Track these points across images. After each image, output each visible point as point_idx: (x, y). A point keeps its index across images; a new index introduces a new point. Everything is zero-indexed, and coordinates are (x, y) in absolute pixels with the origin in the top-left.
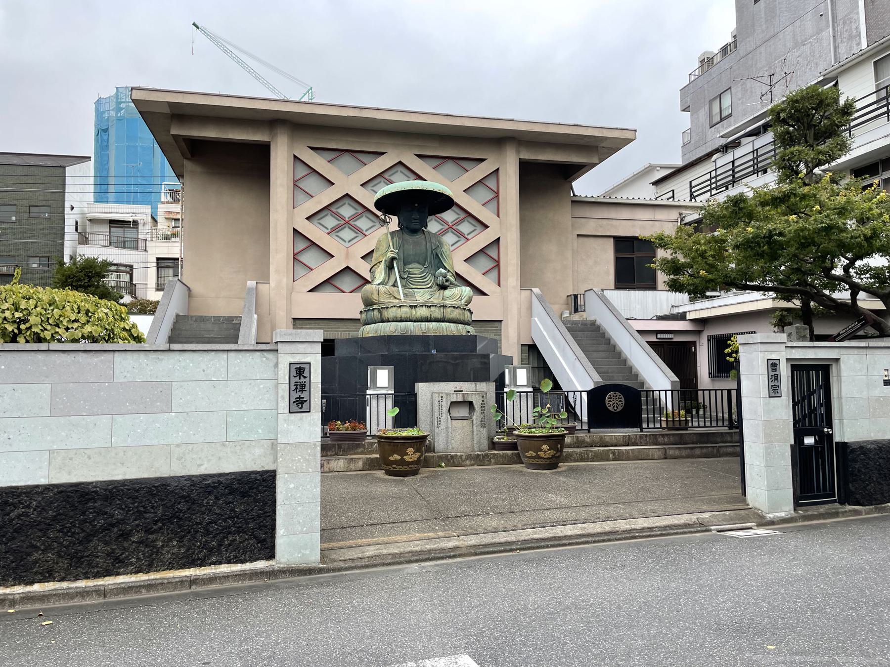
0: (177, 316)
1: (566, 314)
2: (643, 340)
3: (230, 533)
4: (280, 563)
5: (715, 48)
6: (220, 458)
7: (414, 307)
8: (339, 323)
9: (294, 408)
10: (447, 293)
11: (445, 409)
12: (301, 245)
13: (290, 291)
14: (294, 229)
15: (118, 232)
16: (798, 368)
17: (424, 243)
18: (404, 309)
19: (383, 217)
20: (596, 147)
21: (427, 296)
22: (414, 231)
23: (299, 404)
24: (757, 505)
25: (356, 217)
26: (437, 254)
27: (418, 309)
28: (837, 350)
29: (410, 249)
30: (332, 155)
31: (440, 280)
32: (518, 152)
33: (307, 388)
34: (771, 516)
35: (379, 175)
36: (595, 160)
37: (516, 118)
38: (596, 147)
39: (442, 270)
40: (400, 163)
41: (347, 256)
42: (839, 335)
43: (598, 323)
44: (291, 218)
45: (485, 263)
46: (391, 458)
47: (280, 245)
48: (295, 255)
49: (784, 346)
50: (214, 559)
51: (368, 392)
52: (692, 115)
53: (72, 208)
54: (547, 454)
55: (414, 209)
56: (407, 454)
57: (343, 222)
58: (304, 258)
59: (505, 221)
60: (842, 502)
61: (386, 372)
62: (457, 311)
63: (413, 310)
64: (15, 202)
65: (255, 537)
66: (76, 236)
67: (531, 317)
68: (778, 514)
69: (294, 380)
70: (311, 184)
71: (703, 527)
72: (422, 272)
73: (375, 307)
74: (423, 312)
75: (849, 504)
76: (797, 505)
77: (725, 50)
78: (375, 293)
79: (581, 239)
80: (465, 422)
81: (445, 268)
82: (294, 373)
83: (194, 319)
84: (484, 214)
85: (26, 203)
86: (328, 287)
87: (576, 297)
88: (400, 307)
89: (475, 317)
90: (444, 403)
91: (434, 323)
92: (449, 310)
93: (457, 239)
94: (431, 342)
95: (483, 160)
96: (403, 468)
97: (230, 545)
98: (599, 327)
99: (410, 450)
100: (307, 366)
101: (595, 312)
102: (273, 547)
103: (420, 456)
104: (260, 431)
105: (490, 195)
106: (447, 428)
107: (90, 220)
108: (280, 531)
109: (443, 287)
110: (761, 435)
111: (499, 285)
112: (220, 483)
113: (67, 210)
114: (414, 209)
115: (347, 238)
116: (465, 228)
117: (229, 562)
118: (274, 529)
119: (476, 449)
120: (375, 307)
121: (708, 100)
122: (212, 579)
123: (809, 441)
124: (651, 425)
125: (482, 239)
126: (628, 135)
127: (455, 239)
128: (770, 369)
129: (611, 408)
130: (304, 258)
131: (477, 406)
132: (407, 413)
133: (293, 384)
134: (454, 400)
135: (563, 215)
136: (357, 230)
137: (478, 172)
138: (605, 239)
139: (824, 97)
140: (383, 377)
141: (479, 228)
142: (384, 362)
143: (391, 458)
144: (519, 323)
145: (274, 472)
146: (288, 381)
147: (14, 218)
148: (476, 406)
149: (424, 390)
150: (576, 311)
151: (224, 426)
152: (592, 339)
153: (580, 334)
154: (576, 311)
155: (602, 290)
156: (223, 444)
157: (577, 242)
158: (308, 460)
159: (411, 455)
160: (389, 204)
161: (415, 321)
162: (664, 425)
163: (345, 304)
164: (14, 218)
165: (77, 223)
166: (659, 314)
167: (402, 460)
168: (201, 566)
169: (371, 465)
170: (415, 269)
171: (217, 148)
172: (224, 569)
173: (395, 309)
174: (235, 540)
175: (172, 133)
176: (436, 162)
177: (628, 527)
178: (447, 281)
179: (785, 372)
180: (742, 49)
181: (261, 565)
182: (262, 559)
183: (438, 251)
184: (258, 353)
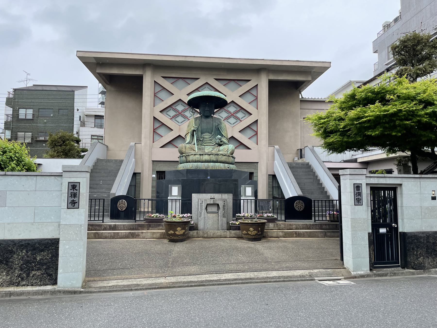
0: (98, 159)
2: (330, 173)
3: (33, 270)
4: (59, 287)
5: (391, 20)
6: (30, 231)
7: (204, 156)
8: (159, 163)
9: (70, 206)
10: (221, 148)
11: (204, 207)
12: (157, 125)
13: (151, 148)
14: (154, 117)
15: (98, 121)
16: (375, 190)
17: (212, 122)
18: (197, 156)
20: (312, 72)
21: (211, 149)
22: (207, 117)
23: (73, 203)
24: (348, 266)
25: (237, 112)
27: (204, 156)
28: (400, 179)
29: (204, 126)
30: (173, 80)
31: (218, 141)
33: (77, 196)
34: (355, 273)
36: (310, 79)
37: (265, 58)
38: (312, 72)
39: (219, 136)
40: (207, 83)
41: (180, 130)
42: (425, 171)
43: (310, 164)
44: (152, 111)
45: (250, 133)
46: (169, 232)
47: (147, 124)
48: (154, 129)
49: (365, 176)
50: (24, 283)
51: (169, 198)
52: (379, 55)
53: (78, 110)
54: (258, 232)
55: (208, 106)
56: (177, 231)
57: (178, 113)
58: (159, 131)
59: (261, 111)
60: (403, 268)
61: (177, 188)
62: (225, 157)
63: (201, 156)
64: (52, 107)
65: (47, 273)
66: (79, 122)
67: (274, 161)
68: (359, 272)
69: (70, 191)
70: (162, 95)
71: (311, 278)
72: (210, 138)
73: (184, 155)
74: (206, 157)
75: (407, 269)
76: (372, 267)
77: (396, 20)
78: (184, 148)
80: (214, 215)
81: (222, 135)
82: (70, 187)
85: (57, 108)
86: (170, 145)
87: (301, 150)
88: (195, 155)
89: (236, 160)
90: (203, 204)
92: (220, 156)
93: (236, 121)
94: (209, 173)
95: (249, 80)
96: (175, 238)
97: (33, 276)
98: (310, 166)
99: (179, 229)
100: (78, 184)
101: (309, 158)
102: (56, 279)
103: (185, 232)
104: (52, 218)
106: (205, 218)
107: (86, 115)
108: (60, 271)
109: (220, 145)
110: (350, 227)
112: (28, 244)
113: (75, 111)
114: (208, 106)
115: (180, 121)
116: (240, 115)
117: (32, 285)
118: (57, 269)
120: (184, 155)
121: (387, 46)
122: (21, 294)
123: (383, 230)
124: (321, 219)
125: (249, 121)
126: (326, 65)
127: (235, 121)
128: (355, 189)
129: (297, 209)
130: (159, 131)
131: (221, 206)
133: (69, 193)
135: (296, 108)
136: (237, 118)
139: (420, 39)
140: (175, 191)
141: (247, 115)
142: (175, 183)
143: (169, 232)
144: (267, 164)
145: (59, 239)
146: (67, 192)
147: (52, 115)
148: (220, 206)
149: (195, 197)
150: (301, 157)
151: (33, 214)
154: (301, 157)
155: (313, 147)
156: (32, 224)
158: (77, 234)
159: (179, 231)
160: (194, 103)
161: (202, 162)
162: (328, 218)
163: (172, 154)
164: (52, 115)
165: (80, 116)
166: (345, 159)
167: (175, 233)
168: (17, 286)
169: (163, 237)
170: (207, 136)
171: (122, 79)
172: (29, 288)
173: (192, 156)
174: (36, 274)
176: (226, 82)
177: (265, 276)
178: (221, 142)
179: (366, 192)
180: (404, 19)
181: (49, 288)
182: (50, 285)
183: (219, 127)
184: (53, 177)
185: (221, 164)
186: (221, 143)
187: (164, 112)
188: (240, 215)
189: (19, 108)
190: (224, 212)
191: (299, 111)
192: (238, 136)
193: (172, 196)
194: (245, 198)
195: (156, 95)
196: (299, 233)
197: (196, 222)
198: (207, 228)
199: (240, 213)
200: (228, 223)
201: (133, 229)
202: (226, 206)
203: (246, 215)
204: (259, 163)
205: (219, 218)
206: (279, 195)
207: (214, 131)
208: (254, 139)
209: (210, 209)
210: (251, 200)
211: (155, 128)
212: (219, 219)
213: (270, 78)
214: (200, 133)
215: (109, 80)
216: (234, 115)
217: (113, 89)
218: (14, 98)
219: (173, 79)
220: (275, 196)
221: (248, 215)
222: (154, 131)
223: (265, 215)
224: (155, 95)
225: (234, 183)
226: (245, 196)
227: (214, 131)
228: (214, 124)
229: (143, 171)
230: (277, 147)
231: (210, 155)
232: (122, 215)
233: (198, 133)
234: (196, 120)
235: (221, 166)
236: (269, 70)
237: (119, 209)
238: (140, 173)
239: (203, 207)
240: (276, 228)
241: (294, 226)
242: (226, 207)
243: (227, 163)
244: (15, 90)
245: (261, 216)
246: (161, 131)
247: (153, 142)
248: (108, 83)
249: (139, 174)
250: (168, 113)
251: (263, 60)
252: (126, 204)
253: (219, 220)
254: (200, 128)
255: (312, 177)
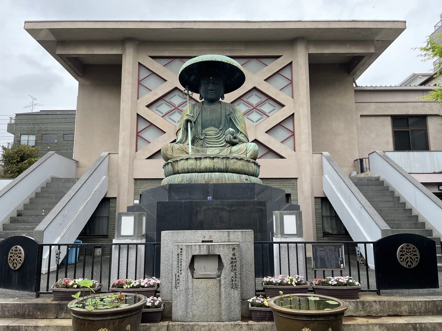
1: (354, 174)
2: (430, 192)
7: (207, 164)
10: (235, 148)
13: (133, 159)
14: (137, 114)
17: (219, 110)
18: (190, 161)
19: (186, 92)
20: (374, 39)
22: (213, 101)
26: (230, 119)
27: (202, 160)
31: (229, 137)
32: (307, 48)
35: (277, 72)
36: (372, 50)
38: (374, 39)
39: (231, 129)
43: (381, 179)
45: (282, 134)
51: (114, 241)
59: (298, 98)
62: (241, 162)
63: (198, 162)
70: (151, 82)
72: (217, 134)
73: (169, 161)
74: (206, 163)
78: (170, 149)
79: (364, 119)
80: (211, 282)
83: (64, 180)
84: (281, 97)
87: (361, 160)
88: (187, 159)
90: (184, 257)
91: (217, 173)
92: (232, 161)
94: (210, 190)
98: (383, 182)
101: (379, 169)
105: (286, 83)
106: (187, 289)
109: (234, 144)
111: (295, 151)
116: (267, 108)
119: (224, 318)
120: (169, 161)
125: (279, 115)
126: (400, 26)
127: (259, 117)
129: (404, 264)
131: (226, 261)
132: (153, 266)
134: (197, 253)
135: (349, 100)
137: (274, 66)
138: (384, 118)
144: (312, 180)
150: (362, 171)
152: (378, 193)
153: (365, 188)
154: (362, 171)
155: (384, 152)
157: (360, 121)
161: (200, 172)
170: (211, 131)
173: (183, 161)
175: (57, 53)
178: (235, 138)
185: (235, 175)
186: (235, 140)
187: (154, 107)
188: (273, 280)
189: (21, 135)
190: (232, 274)
191: (354, 105)
192: (264, 139)
193: (120, 236)
194: (283, 240)
195: (140, 82)
196: (421, 328)
197: (169, 298)
198: (194, 316)
199: (272, 275)
200: (243, 300)
201: (23, 316)
202: (238, 260)
203: (287, 280)
204: (298, 180)
205: (223, 289)
206: (332, 229)
207: (223, 123)
208: (291, 141)
209: (201, 268)
210: (296, 243)
211: (139, 130)
212: (223, 293)
213: (310, 52)
214: (199, 128)
215: (79, 67)
216: (257, 108)
217: (87, 83)
218: (16, 124)
219: (166, 60)
220: (327, 230)
221: (292, 280)
222: (137, 135)
223: (333, 281)
224: (139, 83)
225: (259, 207)
226: (283, 234)
227: (223, 123)
228: (223, 111)
229: (119, 194)
230: (326, 153)
231: (213, 158)
232: (15, 277)
233: (196, 127)
234: (194, 108)
235: (235, 178)
236: (308, 40)
237: (11, 265)
238: (116, 198)
239: (184, 264)
240: (362, 313)
241: (405, 308)
242: (238, 264)
243: (245, 174)
244: (17, 115)
245: (323, 283)
246: (148, 134)
247: (136, 151)
248: (81, 75)
249: (114, 200)
250: (159, 109)
251: (300, 21)
252: (23, 255)
253: (223, 297)
254: (200, 120)
255: (391, 199)
